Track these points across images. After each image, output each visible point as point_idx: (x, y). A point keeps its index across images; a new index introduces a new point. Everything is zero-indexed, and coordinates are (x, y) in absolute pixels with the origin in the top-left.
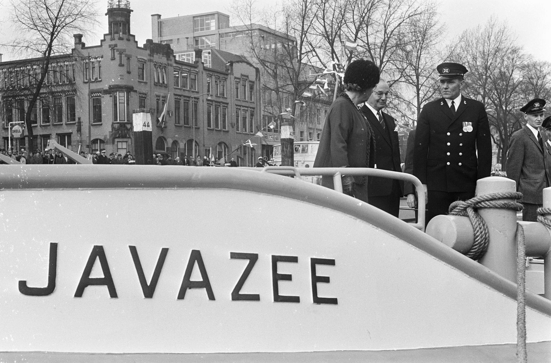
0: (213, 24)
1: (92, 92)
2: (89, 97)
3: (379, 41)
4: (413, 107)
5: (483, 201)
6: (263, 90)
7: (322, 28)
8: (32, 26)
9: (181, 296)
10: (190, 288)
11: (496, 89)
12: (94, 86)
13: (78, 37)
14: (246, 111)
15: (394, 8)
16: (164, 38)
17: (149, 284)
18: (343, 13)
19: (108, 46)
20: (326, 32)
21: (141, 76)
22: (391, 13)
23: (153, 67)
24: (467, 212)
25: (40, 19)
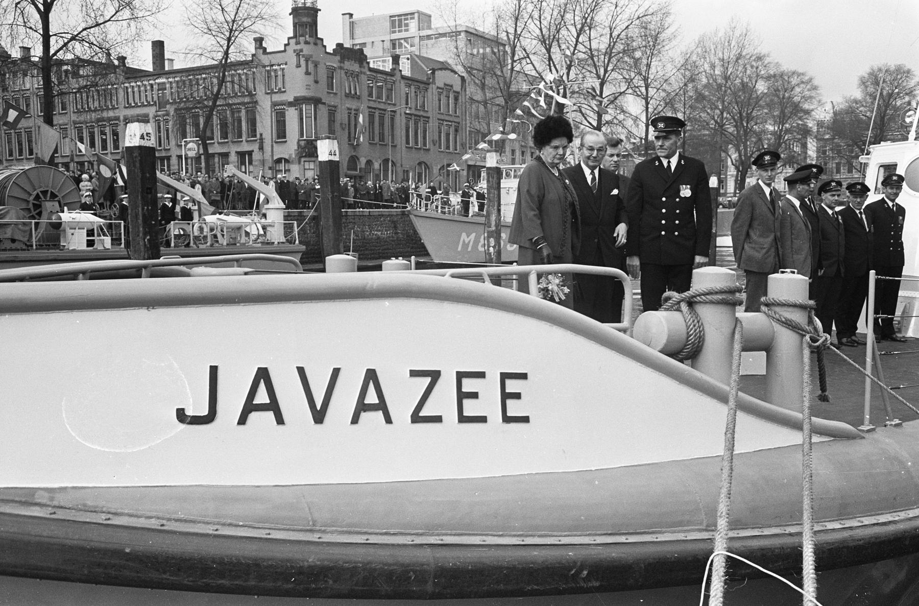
0: (413, 25)
1: (274, 104)
2: (271, 110)
3: (603, 47)
4: (640, 123)
5: (699, 295)
6: (469, 103)
7: (538, 31)
8: (205, 31)
9: (355, 420)
10: (365, 412)
11: (737, 103)
12: (277, 98)
13: (259, 41)
14: (450, 126)
15: (622, 8)
16: (357, 42)
17: (318, 408)
18: (562, 13)
19: (293, 51)
20: (543, 36)
21: (330, 86)
22: (618, 14)
23: (343, 75)
24: (680, 307)
25: (214, 22)
